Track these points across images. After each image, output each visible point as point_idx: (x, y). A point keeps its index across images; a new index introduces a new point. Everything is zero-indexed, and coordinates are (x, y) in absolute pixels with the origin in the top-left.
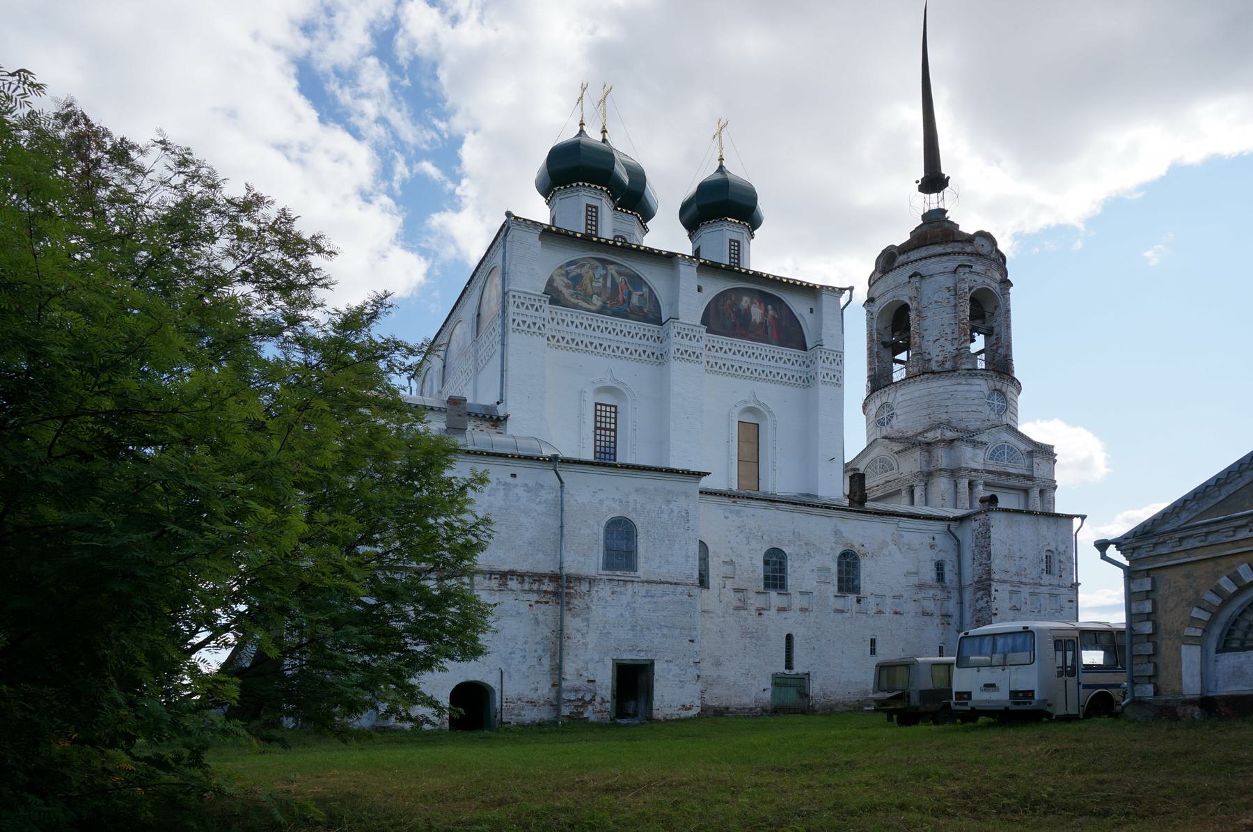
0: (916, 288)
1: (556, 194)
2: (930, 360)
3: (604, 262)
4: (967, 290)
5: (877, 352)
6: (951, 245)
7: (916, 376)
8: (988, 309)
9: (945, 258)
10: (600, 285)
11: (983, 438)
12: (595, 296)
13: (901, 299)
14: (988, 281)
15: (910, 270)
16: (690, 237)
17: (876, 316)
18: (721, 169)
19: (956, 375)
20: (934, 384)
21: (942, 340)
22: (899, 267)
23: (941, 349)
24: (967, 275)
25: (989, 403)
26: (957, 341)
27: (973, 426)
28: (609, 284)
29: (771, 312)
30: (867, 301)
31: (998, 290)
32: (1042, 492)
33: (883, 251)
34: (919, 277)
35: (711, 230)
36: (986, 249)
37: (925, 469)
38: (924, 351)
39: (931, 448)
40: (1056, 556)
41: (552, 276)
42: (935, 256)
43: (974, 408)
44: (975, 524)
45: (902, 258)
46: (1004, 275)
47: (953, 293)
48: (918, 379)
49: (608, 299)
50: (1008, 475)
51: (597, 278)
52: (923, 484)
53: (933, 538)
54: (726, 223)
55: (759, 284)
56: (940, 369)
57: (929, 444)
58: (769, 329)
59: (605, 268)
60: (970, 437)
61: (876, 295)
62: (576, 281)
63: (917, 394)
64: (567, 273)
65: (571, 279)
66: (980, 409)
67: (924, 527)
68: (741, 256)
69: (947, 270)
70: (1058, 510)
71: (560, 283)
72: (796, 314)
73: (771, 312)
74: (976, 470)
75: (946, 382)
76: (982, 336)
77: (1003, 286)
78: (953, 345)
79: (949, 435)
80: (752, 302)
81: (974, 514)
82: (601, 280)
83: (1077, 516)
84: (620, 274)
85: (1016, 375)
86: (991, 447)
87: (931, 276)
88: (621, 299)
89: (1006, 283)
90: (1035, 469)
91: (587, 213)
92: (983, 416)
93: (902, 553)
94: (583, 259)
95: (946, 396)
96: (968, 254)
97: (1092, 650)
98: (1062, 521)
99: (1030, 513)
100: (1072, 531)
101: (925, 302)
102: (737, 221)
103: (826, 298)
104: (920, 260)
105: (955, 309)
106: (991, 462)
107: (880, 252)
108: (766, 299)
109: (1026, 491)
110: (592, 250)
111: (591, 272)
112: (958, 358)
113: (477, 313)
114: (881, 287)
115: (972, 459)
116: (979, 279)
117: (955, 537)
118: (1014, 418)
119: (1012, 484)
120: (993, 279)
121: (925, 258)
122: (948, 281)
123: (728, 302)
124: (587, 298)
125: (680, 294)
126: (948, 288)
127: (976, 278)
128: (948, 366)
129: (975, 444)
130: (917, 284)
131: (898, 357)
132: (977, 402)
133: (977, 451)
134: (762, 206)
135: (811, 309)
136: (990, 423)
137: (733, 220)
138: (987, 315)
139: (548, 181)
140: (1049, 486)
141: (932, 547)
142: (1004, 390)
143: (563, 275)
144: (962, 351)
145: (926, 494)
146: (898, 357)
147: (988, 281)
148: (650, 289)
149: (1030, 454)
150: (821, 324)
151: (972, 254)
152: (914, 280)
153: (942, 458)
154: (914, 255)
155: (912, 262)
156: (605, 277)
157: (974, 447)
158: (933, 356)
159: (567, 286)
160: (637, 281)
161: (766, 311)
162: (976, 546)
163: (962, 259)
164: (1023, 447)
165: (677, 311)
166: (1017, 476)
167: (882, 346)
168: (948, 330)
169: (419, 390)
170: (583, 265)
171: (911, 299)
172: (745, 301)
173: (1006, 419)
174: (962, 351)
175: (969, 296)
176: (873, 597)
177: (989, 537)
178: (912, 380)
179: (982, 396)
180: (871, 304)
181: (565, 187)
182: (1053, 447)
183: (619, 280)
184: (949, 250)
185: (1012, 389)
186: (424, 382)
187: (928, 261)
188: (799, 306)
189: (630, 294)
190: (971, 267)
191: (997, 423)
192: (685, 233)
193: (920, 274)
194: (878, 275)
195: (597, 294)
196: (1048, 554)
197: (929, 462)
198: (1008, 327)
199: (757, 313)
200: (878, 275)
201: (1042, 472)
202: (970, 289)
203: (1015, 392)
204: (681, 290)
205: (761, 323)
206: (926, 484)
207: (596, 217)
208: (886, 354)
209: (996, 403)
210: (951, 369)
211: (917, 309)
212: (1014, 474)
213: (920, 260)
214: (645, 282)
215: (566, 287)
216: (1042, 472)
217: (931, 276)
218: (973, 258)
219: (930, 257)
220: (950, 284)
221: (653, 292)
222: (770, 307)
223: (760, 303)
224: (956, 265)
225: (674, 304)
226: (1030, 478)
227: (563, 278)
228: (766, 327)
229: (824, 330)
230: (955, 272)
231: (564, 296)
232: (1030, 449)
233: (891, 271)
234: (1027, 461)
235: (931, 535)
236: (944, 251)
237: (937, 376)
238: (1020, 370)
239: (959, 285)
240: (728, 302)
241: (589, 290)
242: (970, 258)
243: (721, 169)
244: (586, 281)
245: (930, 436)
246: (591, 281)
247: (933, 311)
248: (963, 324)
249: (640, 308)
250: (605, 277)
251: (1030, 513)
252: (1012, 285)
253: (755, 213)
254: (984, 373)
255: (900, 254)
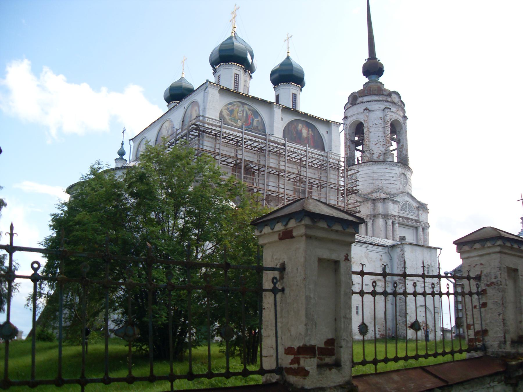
0: (367, 116)
1: (221, 66)
2: (373, 154)
3: (243, 104)
4: (389, 121)
5: (349, 145)
6: (382, 96)
7: (367, 162)
8: (398, 129)
9: (379, 103)
10: (241, 115)
11: (397, 199)
12: (239, 120)
13: (360, 120)
14: (398, 116)
15: (363, 106)
16: (274, 88)
17: (348, 126)
18: (288, 58)
19: (385, 163)
20: (376, 167)
21: (378, 144)
22: (359, 103)
23: (378, 149)
24: (389, 113)
25: (400, 180)
26: (385, 145)
27: (393, 191)
28: (245, 115)
29: (310, 132)
30: (344, 118)
31: (402, 121)
32: (423, 229)
33: (352, 94)
34: (368, 110)
35: (284, 87)
36: (396, 100)
37: (372, 213)
38: (370, 149)
39: (375, 202)
40: (431, 268)
41: (222, 110)
42: (375, 101)
43: (393, 182)
44: (398, 250)
45: (360, 100)
46: (404, 113)
47: (383, 120)
48: (368, 163)
49: (244, 122)
50: (409, 219)
51: (241, 111)
52: (371, 221)
53: (381, 256)
54: (291, 85)
55: (306, 118)
56: (378, 160)
57: (374, 200)
58: (310, 141)
59: (243, 107)
60: (391, 198)
61: (348, 115)
62: (231, 112)
63: (368, 171)
64: (228, 108)
65: (229, 111)
66: (396, 183)
67: (378, 250)
68: (297, 101)
69: (380, 109)
70: (431, 244)
71: (225, 113)
72: (321, 134)
73: (310, 132)
74: (395, 216)
75: (381, 167)
76: (395, 143)
77: (404, 119)
78: (383, 147)
79: (383, 196)
80: (303, 127)
81: (398, 245)
82: (241, 113)
83: (439, 248)
84: (250, 110)
85: (410, 166)
86: (401, 204)
87: (373, 111)
88: (249, 122)
89: (405, 117)
90: (420, 217)
91: (238, 82)
92: (397, 186)
93: (369, 263)
94: (234, 102)
95: (381, 174)
96: (389, 102)
97: (284, 61)
98: (433, 251)
99: (420, 246)
100: (437, 255)
101: (370, 124)
102: (296, 85)
103: (333, 127)
104: (369, 102)
105: (384, 129)
106: (401, 212)
107: (350, 94)
108: (309, 126)
109: (416, 228)
110: (238, 98)
111: (238, 108)
112: (386, 155)
113: (182, 121)
114: (350, 113)
115: (393, 209)
116: (394, 115)
117: (390, 256)
118: (410, 188)
119: (409, 224)
120: (400, 115)
121: (371, 101)
122: (380, 114)
123: (293, 126)
124: (236, 121)
125: (275, 122)
126: (381, 118)
127: (393, 114)
128: (381, 158)
129: (395, 202)
130: (367, 114)
131: (357, 148)
132: (394, 179)
133: (395, 206)
134: (307, 79)
135: (327, 131)
136: (400, 190)
137: (294, 84)
138: (398, 132)
139: (217, 56)
140: (426, 226)
141: (381, 260)
142: (406, 173)
143: (226, 109)
144: (387, 151)
145: (373, 226)
146: (357, 148)
147: (398, 116)
148: (261, 118)
149: (418, 208)
150: (331, 138)
151: (390, 102)
152: (366, 111)
153: (380, 208)
154: (366, 99)
155: (365, 102)
156: (243, 111)
157: (394, 203)
158: (375, 152)
159: (228, 115)
160: (256, 114)
161: (309, 131)
162: (399, 261)
163: (387, 104)
164: (415, 204)
165: (273, 133)
166: (413, 220)
167: (351, 142)
168: (381, 140)
169: (136, 148)
170: (234, 105)
171: (364, 121)
172: (300, 126)
173: (407, 190)
174: (387, 151)
175: (390, 123)
176: (357, 284)
177: (404, 257)
178: (365, 164)
179: (396, 176)
180: (346, 119)
181: (226, 64)
182: (427, 205)
183: (249, 113)
184: (381, 99)
185: (409, 173)
186: (140, 144)
187: (372, 103)
188: (322, 130)
189: (253, 120)
190: (390, 109)
191: (403, 190)
192: (271, 86)
193: (368, 109)
194: (349, 105)
195: (240, 119)
196: (428, 267)
197: (374, 209)
198: (406, 140)
199: (305, 132)
200: (349, 105)
201: (423, 218)
202: (390, 120)
203: (410, 174)
204: (275, 121)
205: (306, 137)
206: (373, 221)
207: (238, 79)
208: (352, 146)
209: (402, 180)
210: (383, 160)
211: (367, 127)
212: (411, 219)
213: (369, 102)
214: (259, 115)
215: (227, 115)
216: (423, 218)
217: (373, 111)
218: (391, 104)
219: (373, 101)
220: (382, 116)
221: (262, 119)
222: (310, 129)
223: (306, 127)
224: (384, 107)
225: (272, 126)
226: (418, 221)
227: (226, 111)
228: (308, 140)
229: (333, 143)
230: (383, 110)
231: (226, 120)
232: (417, 206)
233: (355, 105)
234: (416, 212)
235: (380, 254)
236: (379, 99)
237: (377, 163)
238: (412, 164)
239: (385, 117)
240: (293, 126)
241: (237, 117)
242: (390, 104)
243: (288, 58)
244: (235, 113)
245: (375, 195)
246: (238, 112)
247: (374, 129)
248: (388, 137)
249: (257, 127)
250: (243, 111)
251: (420, 246)
252: (407, 119)
253: (294, 69)
254: (397, 164)
255: (359, 97)
